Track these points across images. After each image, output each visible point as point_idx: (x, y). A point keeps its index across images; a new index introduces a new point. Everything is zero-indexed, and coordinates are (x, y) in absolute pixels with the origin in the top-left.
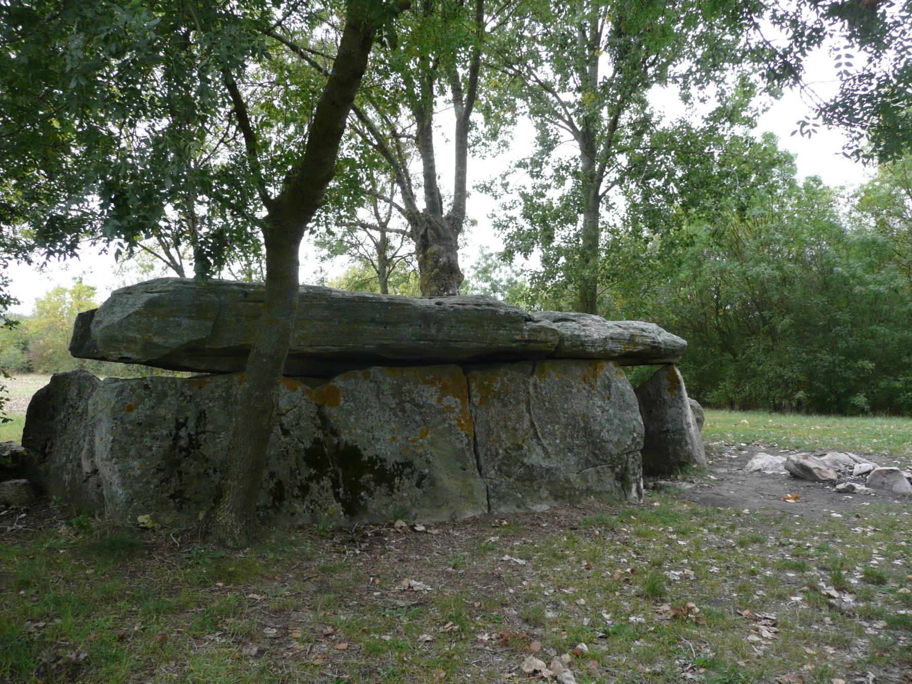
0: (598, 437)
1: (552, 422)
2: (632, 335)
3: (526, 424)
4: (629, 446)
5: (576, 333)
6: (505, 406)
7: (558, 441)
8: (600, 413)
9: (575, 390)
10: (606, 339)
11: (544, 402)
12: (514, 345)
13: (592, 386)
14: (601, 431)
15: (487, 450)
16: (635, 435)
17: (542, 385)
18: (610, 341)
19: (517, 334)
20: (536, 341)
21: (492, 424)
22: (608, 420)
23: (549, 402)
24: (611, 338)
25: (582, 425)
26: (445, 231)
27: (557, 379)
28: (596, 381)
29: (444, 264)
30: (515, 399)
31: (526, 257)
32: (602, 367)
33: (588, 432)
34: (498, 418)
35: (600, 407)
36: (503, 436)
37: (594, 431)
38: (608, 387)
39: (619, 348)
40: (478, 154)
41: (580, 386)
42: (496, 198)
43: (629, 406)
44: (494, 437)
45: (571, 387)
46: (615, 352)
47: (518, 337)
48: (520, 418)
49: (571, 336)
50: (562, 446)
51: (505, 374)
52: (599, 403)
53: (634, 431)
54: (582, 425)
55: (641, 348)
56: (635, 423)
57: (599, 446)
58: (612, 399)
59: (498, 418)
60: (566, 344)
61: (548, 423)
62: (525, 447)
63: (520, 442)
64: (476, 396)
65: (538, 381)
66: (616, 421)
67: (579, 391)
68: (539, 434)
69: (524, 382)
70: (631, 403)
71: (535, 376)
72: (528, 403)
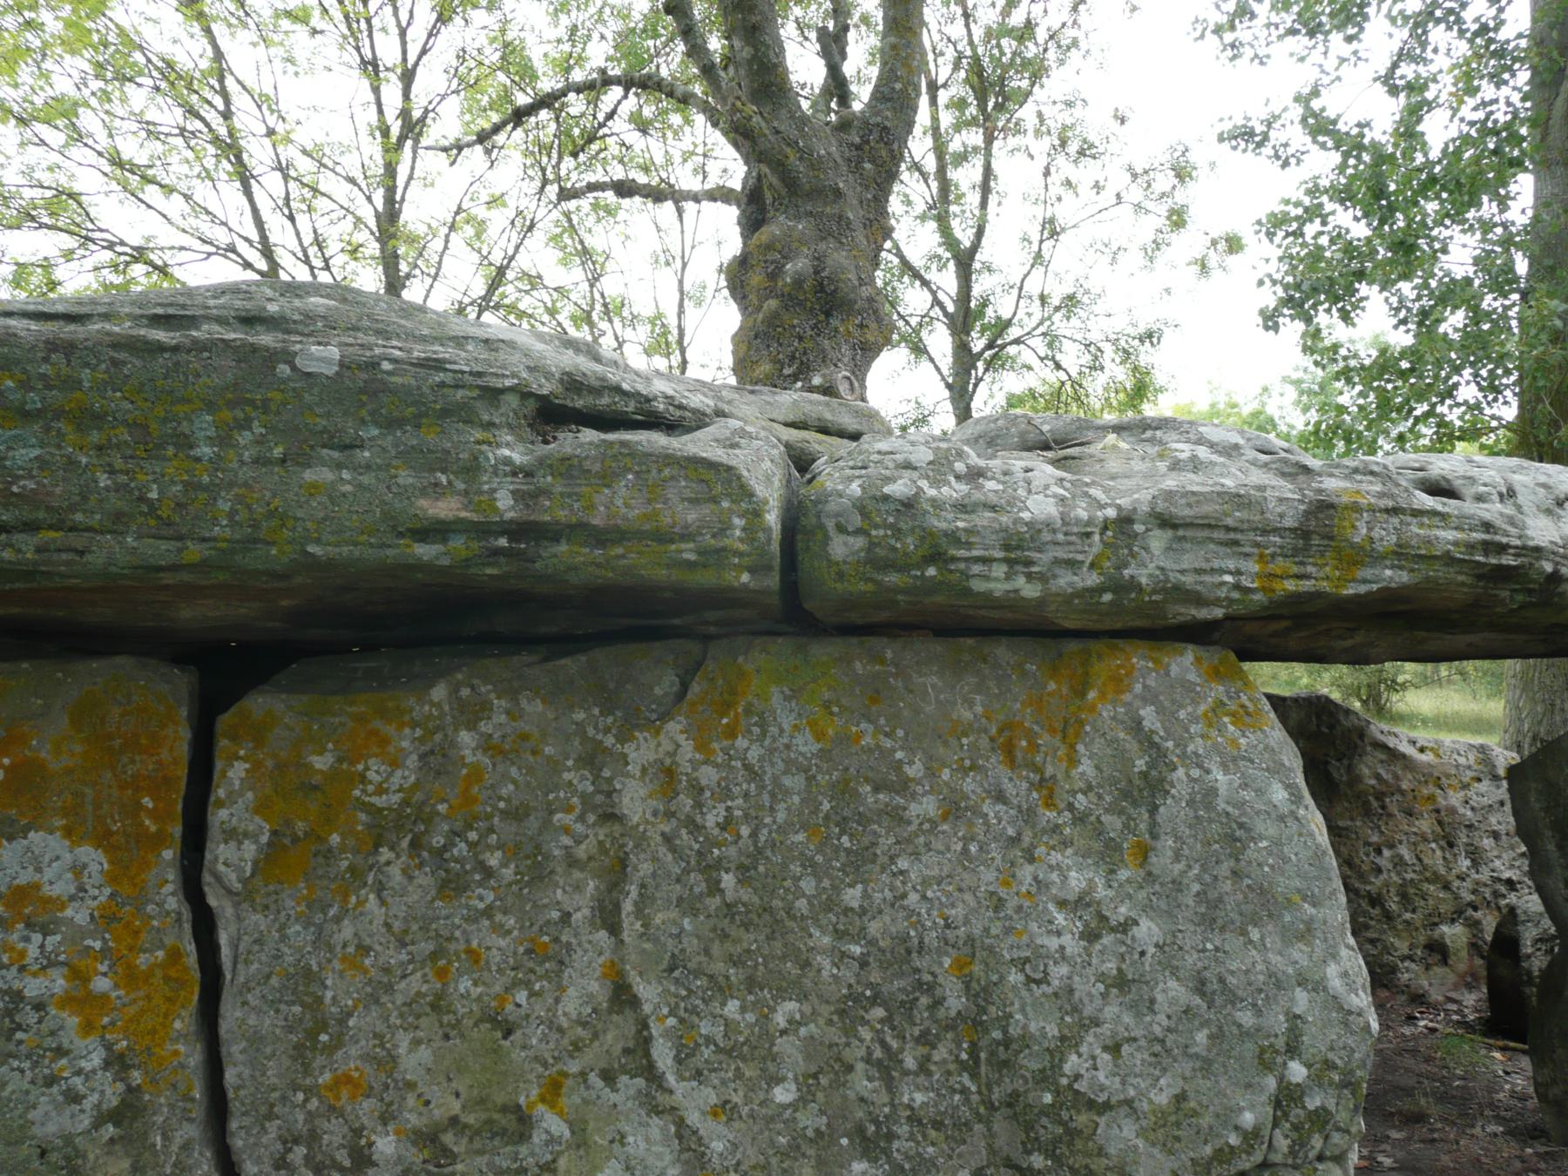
0: (1045, 1078)
1: (751, 984)
2: (1323, 506)
3: (582, 989)
4: (1252, 1137)
5: (899, 488)
6: (451, 886)
7: (783, 1094)
8: (1072, 944)
9: (927, 806)
10: (1125, 521)
11: (711, 869)
12: (425, 551)
13: (1047, 788)
14: (1068, 1042)
15: (290, 1140)
16: (1297, 1071)
17: (708, 775)
18: (1158, 541)
19: (437, 491)
20: (580, 531)
21: (337, 990)
22: (1121, 982)
23: (744, 873)
24: (1165, 522)
25: (955, 1002)
26: (815, 165)
27: (806, 745)
28: (1073, 761)
29: (798, 282)
30: (512, 851)
31: (1346, 317)
32: (1119, 683)
33: (986, 1044)
34: (396, 957)
35: (1077, 904)
36: (414, 1060)
37: (1026, 1040)
38: (1149, 789)
39: (1231, 577)
40: (1248, 52)
41: (969, 784)
42: (1286, 164)
43: (1265, 904)
44: (351, 1059)
45: (904, 786)
46: (1198, 600)
47: (445, 508)
48: (546, 956)
49: (861, 507)
50: (810, 1120)
51: (472, 714)
52: (1077, 881)
53: (1292, 1050)
54: (955, 1002)
55: (1391, 576)
56: (1302, 1000)
57: (1049, 1130)
58: (1162, 861)
59: (396, 957)
60: (841, 548)
61: (722, 990)
62: (552, 1124)
63: (527, 1096)
64: (231, 835)
65: (688, 751)
66: (1172, 992)
67: (954, 809)
68: (663, 1054)
69: (592, 758)
70: (1286, 884)
71: (674, 727)
72: (617, 872)
